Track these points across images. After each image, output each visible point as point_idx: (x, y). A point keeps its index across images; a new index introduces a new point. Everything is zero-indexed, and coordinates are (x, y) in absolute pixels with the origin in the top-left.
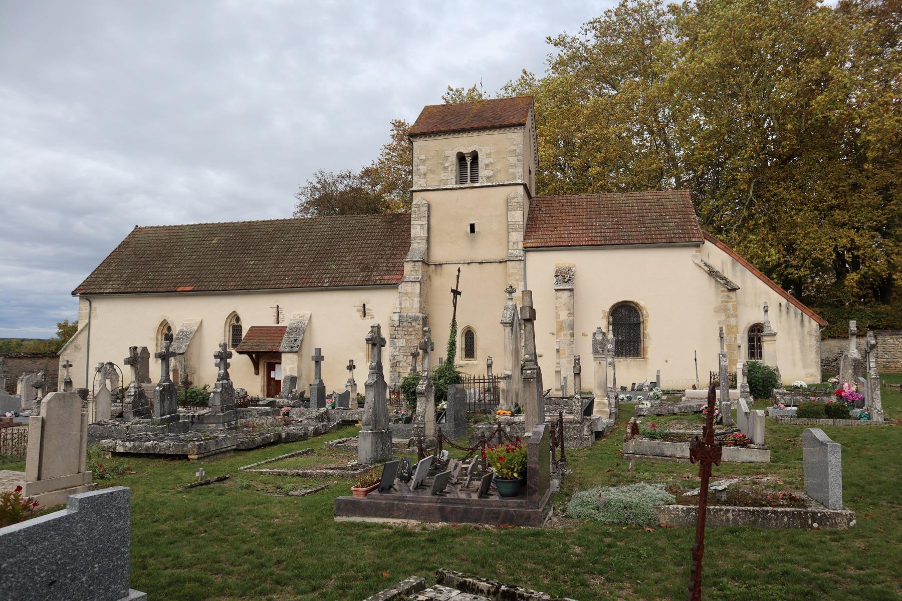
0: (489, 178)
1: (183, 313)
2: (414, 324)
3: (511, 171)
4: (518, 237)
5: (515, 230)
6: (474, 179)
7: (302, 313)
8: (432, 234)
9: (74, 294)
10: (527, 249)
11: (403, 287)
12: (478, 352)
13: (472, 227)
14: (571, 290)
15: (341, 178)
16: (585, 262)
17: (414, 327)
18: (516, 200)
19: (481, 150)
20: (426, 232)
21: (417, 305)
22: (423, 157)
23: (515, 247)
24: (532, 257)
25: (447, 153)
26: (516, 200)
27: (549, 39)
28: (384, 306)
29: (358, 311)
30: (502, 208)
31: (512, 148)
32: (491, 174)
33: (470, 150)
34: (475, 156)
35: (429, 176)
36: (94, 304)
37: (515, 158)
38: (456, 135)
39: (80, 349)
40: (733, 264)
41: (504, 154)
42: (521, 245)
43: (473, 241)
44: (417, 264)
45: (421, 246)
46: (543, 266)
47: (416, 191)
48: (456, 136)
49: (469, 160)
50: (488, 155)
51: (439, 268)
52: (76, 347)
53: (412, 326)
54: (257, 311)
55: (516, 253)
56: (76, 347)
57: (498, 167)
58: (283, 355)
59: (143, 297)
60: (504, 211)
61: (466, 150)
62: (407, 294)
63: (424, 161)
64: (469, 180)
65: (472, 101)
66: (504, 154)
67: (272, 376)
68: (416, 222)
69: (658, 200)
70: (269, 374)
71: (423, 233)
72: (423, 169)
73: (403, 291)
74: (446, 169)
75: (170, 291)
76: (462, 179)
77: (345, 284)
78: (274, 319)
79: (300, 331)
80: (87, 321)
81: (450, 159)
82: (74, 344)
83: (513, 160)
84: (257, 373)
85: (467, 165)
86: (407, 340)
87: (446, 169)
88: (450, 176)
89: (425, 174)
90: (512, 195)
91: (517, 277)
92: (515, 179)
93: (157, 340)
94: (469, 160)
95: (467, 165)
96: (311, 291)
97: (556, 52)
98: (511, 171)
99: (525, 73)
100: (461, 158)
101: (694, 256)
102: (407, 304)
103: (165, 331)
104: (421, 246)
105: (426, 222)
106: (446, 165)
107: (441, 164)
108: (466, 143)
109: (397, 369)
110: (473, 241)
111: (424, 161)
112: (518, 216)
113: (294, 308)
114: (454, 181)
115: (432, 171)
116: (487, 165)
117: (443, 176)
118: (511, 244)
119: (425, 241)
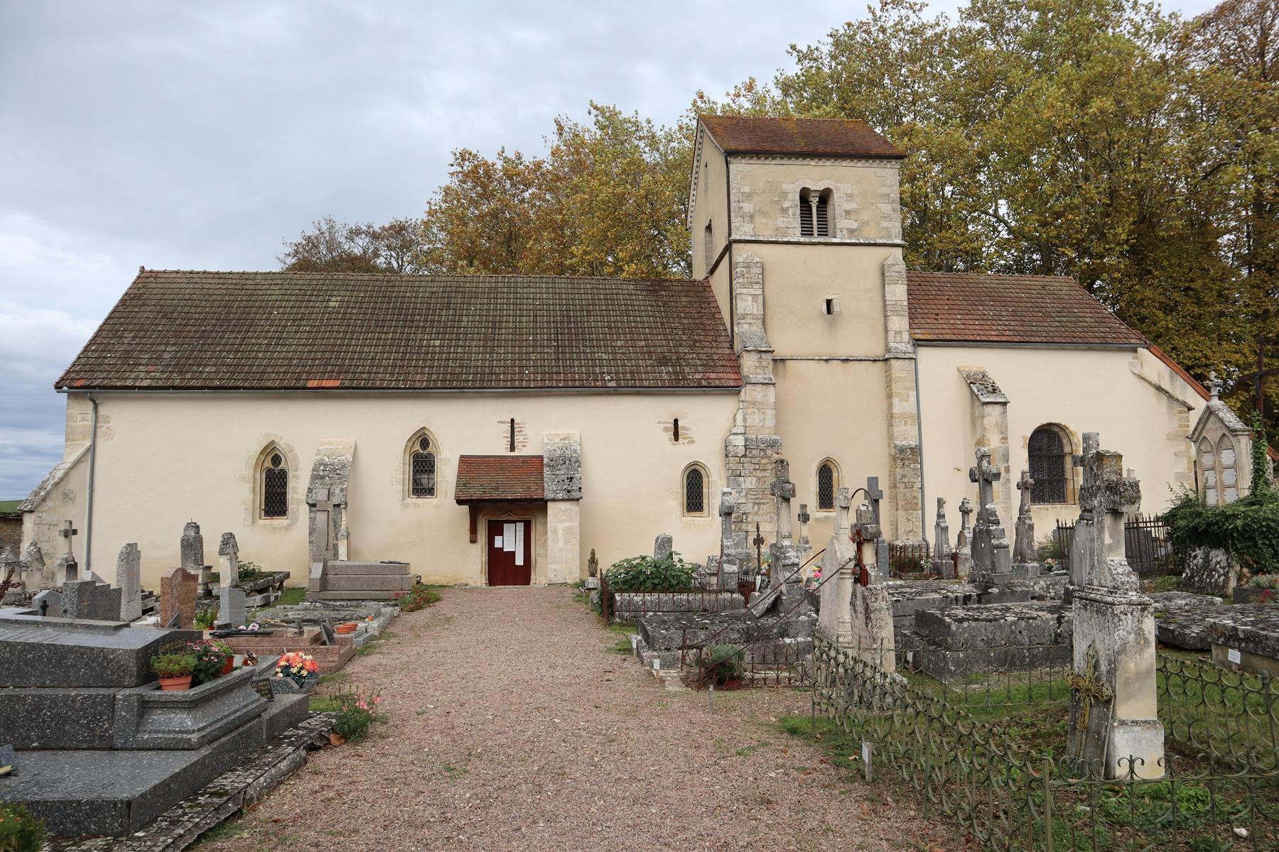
0: (851, 231)
1: (314, 432)
2: (769, 452)
3: (885, 224)
4: (900, 323)
5: (897, 313)
6: (823, 231)
7: (563, 431)
8: (768, 312)
9: (58, 387)
10: (918, 343)
11: (747, 393)
12: (839, 500)
13: (829, 302)
14: (1004, 404)
15: (354, 233)
16: (1000, 365)
17: (769, 458)
18: (896, 268)
19: (838, 189)
20: (761, 307)
21: (770, 422)
22: (747, 189)
23: (898, 339)
24: (925, 354)
25: (786, 187)
26: (896, 268)
27: (793, 47)
28: (710, 423)
29: (666, 430)
30: (874, 280)
31: (884, 190)
32: (854, 225)
33: (821, 186)
34: (825, 197)
35: (758, 219)
36: (103, 410)
37: (889, 207)
38: (800, 161)
39: (73, 500)
40: (1172, 377)
41: (867, 195)
42: (906, 337)
43: (832, 326)
44: (764, 356)
45: (754, 328)
46: (942, 369)
47: (739, 241)
48: (762, 161)
49: (814, 202)
50: (849, 197)
51: (780, 365)
52: (66, 495)
53: (766, 456)
54: (469, 429)
55: (903, 347)
56: (66, 495)
57: (865, 216)
58: (550, 505)
59: (223, 399)
60: (878, 282)
61: (817, 185)
62: (754, 403)
63: (749, 196)
64: (815, 233)
65: (755, 119)
66: (867, 195)
67: (498, 544)
68: (744, 291)
69: (1043, 287)
70: (491, 542)
71: (756, 309)
72: (747, 207)
73: (748, 398)
74: (784, 211)
75: (292, 387)
76: (807, 230)
77: (646, 383)
78: (506, 443)
79: (569, 463)
80: (88, 443)
81: (790, 196)
82: (61, 489)
83: (886, 208)
84: (473, 541)
85: (815, 209)
86: (759, 479)
87: (784, 211)
88: (791, 224)
89: (752, 217)
90: (890, 261)
91: (907, 384)
92: (890, 237)
93: (255, 480)
94: (814, 202)
95: (815, 209)
96: (579, 394)
97: (793, 69)
98: (885, 224)
99: (702, 97)
100: (804, 195)
101: (1131, 364)
102: (755, 419)
103: (268, 464)
104: (754, 328)
105: (760, 292)
106: (786, 205)
107: (777, 202)
108: (816, 175)
109: (744, 526)
110: (832, 326)
111: (749, 196)
112: (899, 292)
113: (547, 425)
114: (799, 231)
115: (764, 214)
116: (848, 212)
117: (781, 221)
118: (891, 334)
119: (760, 322)
